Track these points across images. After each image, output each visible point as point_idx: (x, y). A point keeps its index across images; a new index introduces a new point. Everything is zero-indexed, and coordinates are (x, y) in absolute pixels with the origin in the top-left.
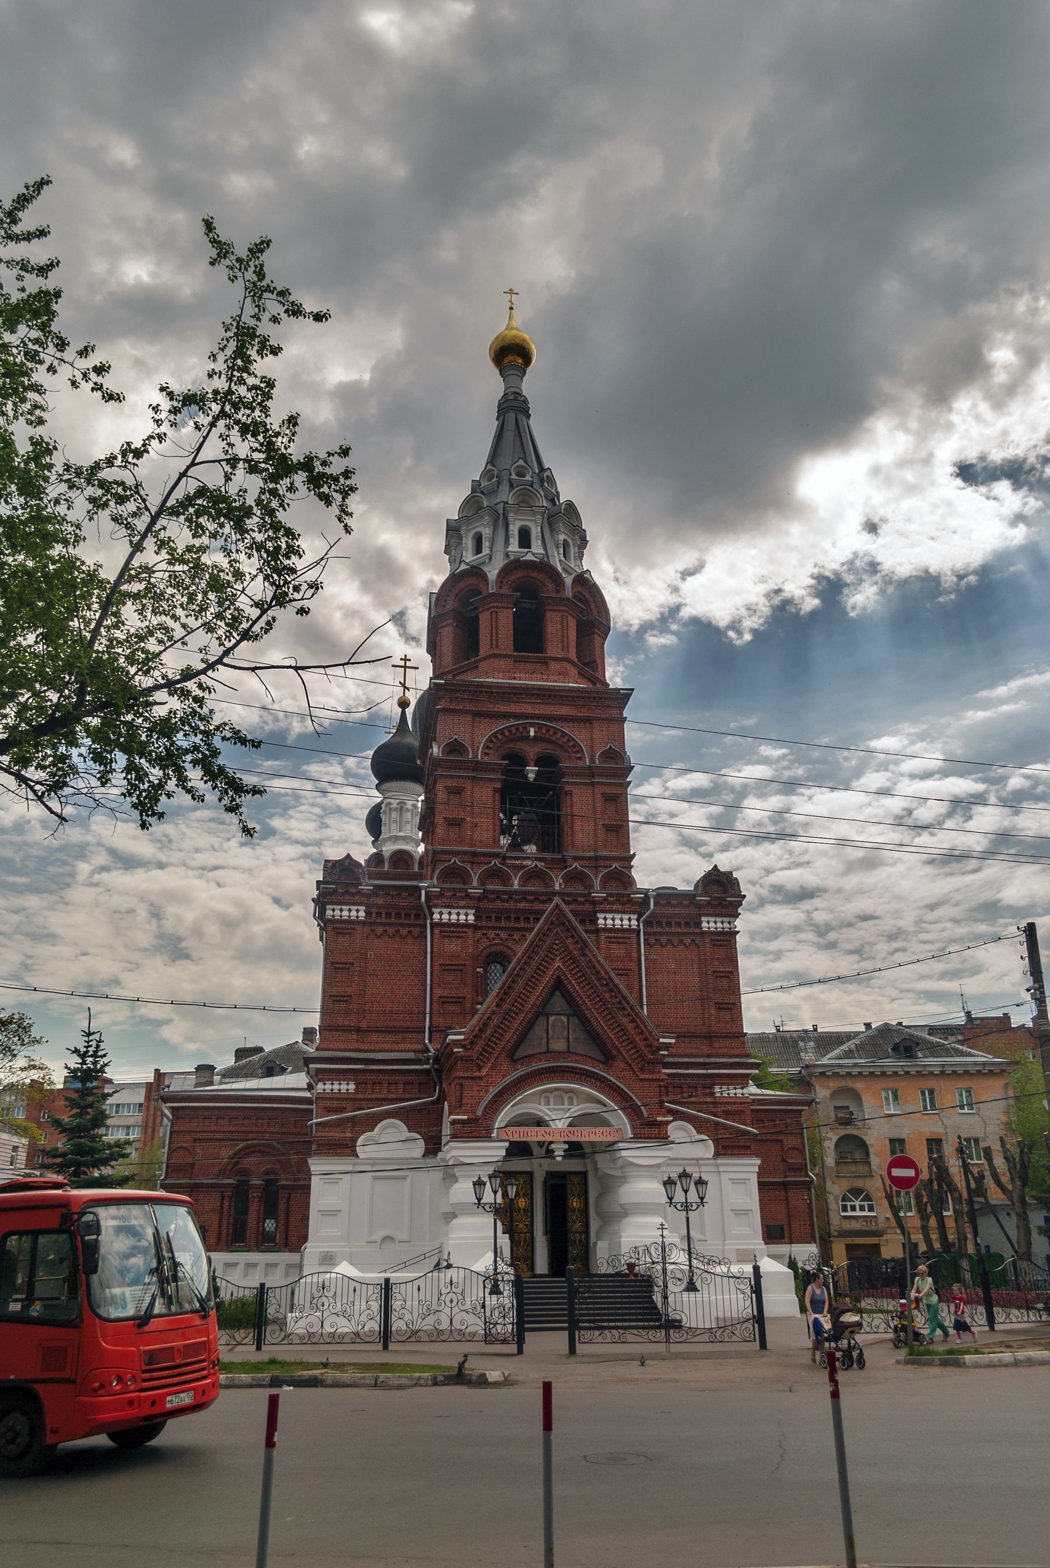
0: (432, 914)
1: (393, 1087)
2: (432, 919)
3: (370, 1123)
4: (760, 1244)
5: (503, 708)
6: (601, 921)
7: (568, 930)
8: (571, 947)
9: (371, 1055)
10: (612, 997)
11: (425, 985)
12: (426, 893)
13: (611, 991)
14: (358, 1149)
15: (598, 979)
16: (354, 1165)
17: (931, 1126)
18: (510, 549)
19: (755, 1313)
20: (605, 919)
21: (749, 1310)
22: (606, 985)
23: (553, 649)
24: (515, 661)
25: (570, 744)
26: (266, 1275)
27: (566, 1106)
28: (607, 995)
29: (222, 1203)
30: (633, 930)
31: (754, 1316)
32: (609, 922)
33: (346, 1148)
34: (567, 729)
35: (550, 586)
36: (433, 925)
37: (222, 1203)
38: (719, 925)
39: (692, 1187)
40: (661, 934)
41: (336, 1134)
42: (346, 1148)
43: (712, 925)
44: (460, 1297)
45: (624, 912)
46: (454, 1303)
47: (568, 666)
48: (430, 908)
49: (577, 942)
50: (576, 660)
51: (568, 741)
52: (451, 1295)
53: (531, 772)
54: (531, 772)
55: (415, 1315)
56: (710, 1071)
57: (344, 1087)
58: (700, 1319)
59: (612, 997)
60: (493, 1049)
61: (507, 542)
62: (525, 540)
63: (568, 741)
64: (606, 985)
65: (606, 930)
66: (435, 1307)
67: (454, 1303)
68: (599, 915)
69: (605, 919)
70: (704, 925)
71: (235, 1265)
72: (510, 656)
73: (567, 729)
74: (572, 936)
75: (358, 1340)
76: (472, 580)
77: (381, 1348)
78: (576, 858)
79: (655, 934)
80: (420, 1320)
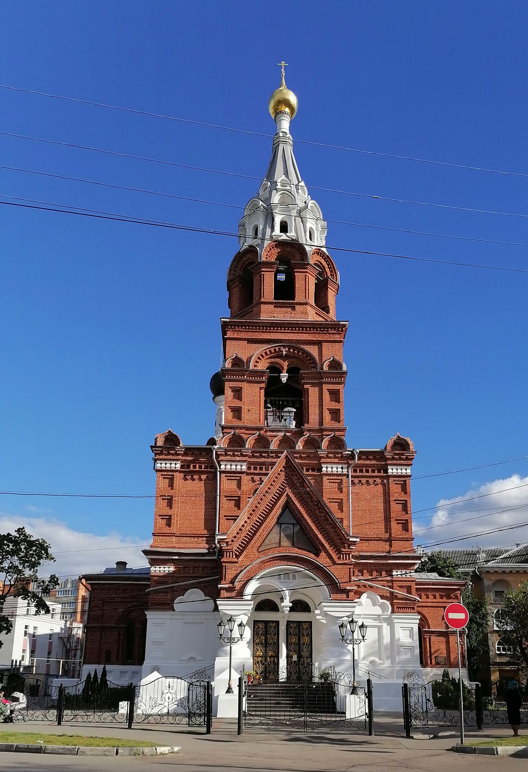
0: (220, 465)
1: (196, 570)
2: (220, 469)
3: (183, 591)
4: (419, 667)
5: (266, 336)
6: (324, 469)
7: (293, 471)
8: (295, 481)
9: (182, 551)
10: (320, 512)
11: (216, 509)
12: (216, 453)
13: (319, 509)
14: (175, 605)
15: (312, 501)
16: (172, 615)
17: (277, 487)
18: (274, 234)
19: (367, 712)
20: (327, 468)
21: (363, 709)
22: (317, 505)
23: (299, 297)
24: (275, 307)
25: (308, 358)
26: (132, 678)
27: (291, 580)
28: (317, 512)
29: (119, 638)
30: (344, 475)
31: (366, 714)
32: (329, 469)
33: (168, 606)
34: (307, 348)
35: (298, 256)
36: (221, 472)
37: (119, 638)
38: (399, 471)
39: (357, 630)
40: (362, 477)
41: (161, 597)
42: (168, 606)
43: (395, 471)
44: (174, 696)
45: (338, 463)
46: (171, 699)
47: (308, 308)
48: (219, 462)
49: (299, 478)
50: (314, 304)
51: (307, 356)
52: (169, 694)
53: (284, 377)
54: (284, 377)
55: (148, 706)
56: (390, 561)
57: (167, 569)
58: (215, 730)
59: (320, 512)
60: (242, 542)
61: (273, 229)
62: (284, 228)
63: (307, 356)
64: (317, 505)
65: (327, 475)
66: (159, 702)
67: (171, 699)
68: (323, 466)
69: (327, 468)
70: (390, 471)
71: (126, 672)
72: (271, 303)
73: (307, 348)
74: (296, 475)
75: (115, 721)
76: (250, 256)
77: (127, 727)
78: (309, 430)
79: (358, 477)
80: (150, 710)
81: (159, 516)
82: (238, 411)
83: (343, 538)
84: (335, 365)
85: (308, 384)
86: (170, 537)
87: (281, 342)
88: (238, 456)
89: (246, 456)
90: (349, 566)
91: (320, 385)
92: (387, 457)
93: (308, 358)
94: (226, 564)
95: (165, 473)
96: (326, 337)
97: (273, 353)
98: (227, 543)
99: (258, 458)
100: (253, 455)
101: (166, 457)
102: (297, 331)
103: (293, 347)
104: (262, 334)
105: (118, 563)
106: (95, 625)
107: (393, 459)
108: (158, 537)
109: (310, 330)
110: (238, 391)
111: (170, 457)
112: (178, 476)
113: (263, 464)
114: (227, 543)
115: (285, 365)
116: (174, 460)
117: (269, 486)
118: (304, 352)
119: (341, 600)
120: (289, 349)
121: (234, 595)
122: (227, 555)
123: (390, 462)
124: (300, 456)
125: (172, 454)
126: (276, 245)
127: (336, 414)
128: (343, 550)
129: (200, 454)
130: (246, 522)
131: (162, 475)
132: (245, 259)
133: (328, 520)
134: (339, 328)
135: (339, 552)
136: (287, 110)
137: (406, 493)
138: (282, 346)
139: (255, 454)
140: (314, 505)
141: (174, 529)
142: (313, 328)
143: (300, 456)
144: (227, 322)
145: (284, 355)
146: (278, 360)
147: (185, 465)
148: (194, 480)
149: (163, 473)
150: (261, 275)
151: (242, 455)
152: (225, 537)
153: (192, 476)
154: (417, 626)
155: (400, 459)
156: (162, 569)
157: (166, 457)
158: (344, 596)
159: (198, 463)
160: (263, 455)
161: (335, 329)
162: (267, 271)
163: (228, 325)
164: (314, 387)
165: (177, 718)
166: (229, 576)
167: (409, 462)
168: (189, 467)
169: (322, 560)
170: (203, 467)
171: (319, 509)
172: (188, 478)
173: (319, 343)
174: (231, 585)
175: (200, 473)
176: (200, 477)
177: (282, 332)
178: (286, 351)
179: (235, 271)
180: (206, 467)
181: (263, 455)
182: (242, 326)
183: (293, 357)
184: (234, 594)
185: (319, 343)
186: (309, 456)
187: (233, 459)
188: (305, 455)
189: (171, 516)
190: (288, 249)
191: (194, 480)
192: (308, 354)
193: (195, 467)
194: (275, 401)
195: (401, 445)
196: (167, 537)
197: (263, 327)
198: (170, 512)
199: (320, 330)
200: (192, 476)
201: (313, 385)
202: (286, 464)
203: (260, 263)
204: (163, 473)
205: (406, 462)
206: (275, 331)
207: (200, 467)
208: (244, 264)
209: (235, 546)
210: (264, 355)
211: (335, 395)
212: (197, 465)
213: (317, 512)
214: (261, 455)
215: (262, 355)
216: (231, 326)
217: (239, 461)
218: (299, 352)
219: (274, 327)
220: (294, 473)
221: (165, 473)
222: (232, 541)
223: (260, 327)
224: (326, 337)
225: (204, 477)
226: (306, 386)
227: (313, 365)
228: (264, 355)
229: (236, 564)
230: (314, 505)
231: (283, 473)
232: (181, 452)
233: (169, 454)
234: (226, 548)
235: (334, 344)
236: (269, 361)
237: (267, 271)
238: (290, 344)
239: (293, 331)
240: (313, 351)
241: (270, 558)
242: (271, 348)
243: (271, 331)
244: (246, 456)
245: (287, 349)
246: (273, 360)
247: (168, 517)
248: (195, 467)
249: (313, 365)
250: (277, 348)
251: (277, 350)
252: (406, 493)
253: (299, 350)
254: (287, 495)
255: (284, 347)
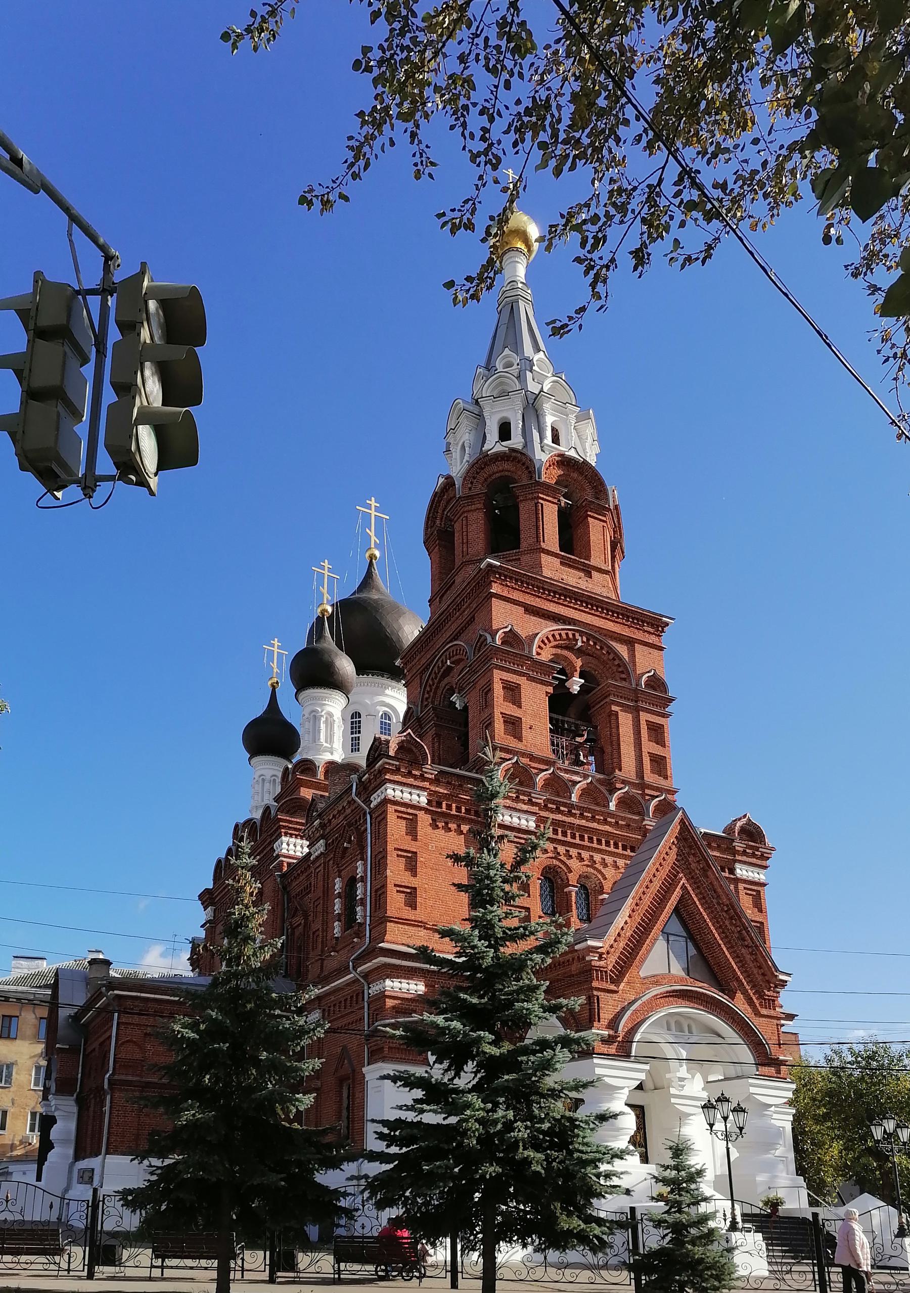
8: (693, 866)
15: (718, 904)
28: (727, 923)
63: (614, 659)
70: (738, 871)
81: (395, 885)
82: (513, 724)
83: (769, 973)
84: (656, 683)
85: (618, 704)
86: (416, 929)
87: (574, 625)
88: (523, 802)
89: (537, 804)
90: (775, 1021)
91: (636, 711)
92: (737, 848)
93: (616, 663)
94: (599, 993)
95: (402, 809)
96: (639, 635)
97: (564, 640)
98: (601, 955)
99: (552, 812)
100: (546, 806)
101: (404, 780)
102: (598, 613)
103: (594, 637)
104: (547, 603)
105: (93, 962)
106: (130, 1078)
107: (744, 853)
108: (396, 925)
109: (618, 617)
110: (513, 690)
111: (411, 781)
112: (424, 819)
113: (571, 826)
114: (601, 955)
115: (578, 663)
116: (418, 787)
117: (657, 865)
118: (611, 650)
119: (769, 1077)
120: (588, 640)
121: (613, 1051)
122: (597, 977)
123: (739, 858)
124: (617, 823)
125: (415, 777)
126: (557, 462)
127: (659, 764)
128: (767, 993)
129: (460, 786)
130: (626, 923)
131: (396, 811)
132: (494, 468)
133: (744, 940)
134: (658, 626)
135: (761, 996)
136: (520, 245)
137: (760, 911)
138: (577, 631)
139: (550, 806)
140: (722, 910)
141: (418, 915)
142: (622, 615)
143: (617, 823)
144: (495, 566)
145: (577, 647)
146: (565, 653)
147: (435, 800)
148: (450, 830)
149: (399, 808)
150: (536, 507)
151: (530, 802)
152: (600, 945)
153: (447, 823)
154: (790, 1127)
155: (753, 855)
156: (405, 985)
157: (404, 780)
158: (772, 1070)
159: (456, 802)
160: (562, 808)
161: (652, 626)
162: (549, 501)
163: (495, 573)
164: (626, 712)
165: (568, 1272)
166: (606, 1015)
167: (763, 863)
168: (439, 805)
169: (739, 1005)
170: (463, 810)
171: (731, 918)
172: (453, 829)
173: (630, 642)
174: (612, 1032)
175: (459, 820)
176: (459, 826)
177: (576, 609)
178: (583, 642)
179: (472, 483)
180: (468, 811)
181: (562, 808)
182: (517, 580)
183: (589, 655)
184: (612, 1050)
185: (630, 642)
186: (629, 825)
187: (514, 805)
188: (624, 823)
189: (415, 888)
190: (575, 475)
191: (450, 830)
192: (617, 656)
193: (449, 807)
194: (557, 720)
195: (752, 833)
196: (411, 928)
197: (549, 591)
198: (413, 882)
199: (633, 622)
200: (447, 823)
201: (626, 708)
202: (680, 833)
203: (538, 484)
204: (399, 808)
205: (759, 862)
206: (566, 603)
207: (458, 809)
208: (490, 476)
209: (610, 963)
210: (551, 638)
211: (657, 733)
212: (454, 805)
213: (727, 923)
214: (558, 808)
215: (547, 638)
216: (500, 575)
217: (526, 812)
218: (602, 648)
219: (566, 597)
220: (693, 852)
221: (402, 809)
222: (608, 953)
223: (544, 589)
224: (639, 635)
225: (465, 828)
226: (614, 708)
227: (623, 676)
228: (551, 638)
229: (615, 995)
230: (722, 910)
231: (675, 849)
232: (430, 776)
233: (410, 774)
234: (598, 964)
235: (651, 650)
236: (554, 651)
237: (549, 501)
238: (593, 634)
239: (593, 612)
240: (622, 650)
241: (667, 992)
242: (563, 630)
243: (561, 601)
244: (537, 804)
245: (585, 639)
246: (559, 651)
247: (409, 891)
248: (449, 807)
249: (623, 676)
250: (570, 632)
251: (571, 636)
252: (760, 911)
253: (604, 645)
254: (684, 888)
255: (582, 634)
